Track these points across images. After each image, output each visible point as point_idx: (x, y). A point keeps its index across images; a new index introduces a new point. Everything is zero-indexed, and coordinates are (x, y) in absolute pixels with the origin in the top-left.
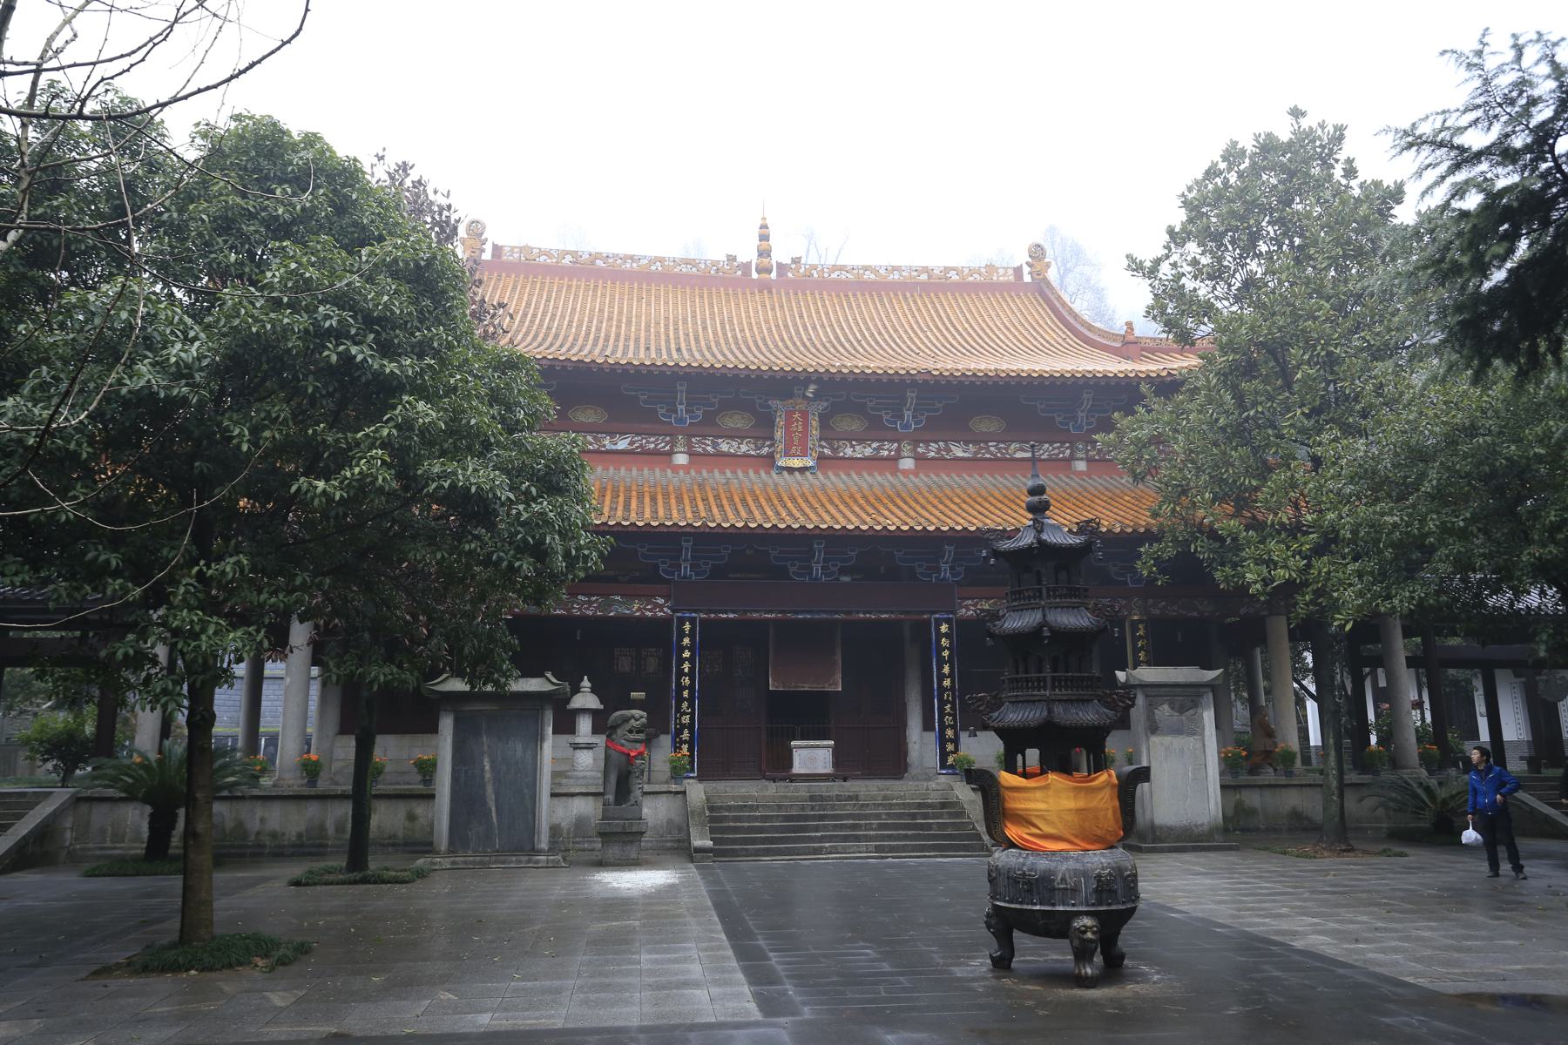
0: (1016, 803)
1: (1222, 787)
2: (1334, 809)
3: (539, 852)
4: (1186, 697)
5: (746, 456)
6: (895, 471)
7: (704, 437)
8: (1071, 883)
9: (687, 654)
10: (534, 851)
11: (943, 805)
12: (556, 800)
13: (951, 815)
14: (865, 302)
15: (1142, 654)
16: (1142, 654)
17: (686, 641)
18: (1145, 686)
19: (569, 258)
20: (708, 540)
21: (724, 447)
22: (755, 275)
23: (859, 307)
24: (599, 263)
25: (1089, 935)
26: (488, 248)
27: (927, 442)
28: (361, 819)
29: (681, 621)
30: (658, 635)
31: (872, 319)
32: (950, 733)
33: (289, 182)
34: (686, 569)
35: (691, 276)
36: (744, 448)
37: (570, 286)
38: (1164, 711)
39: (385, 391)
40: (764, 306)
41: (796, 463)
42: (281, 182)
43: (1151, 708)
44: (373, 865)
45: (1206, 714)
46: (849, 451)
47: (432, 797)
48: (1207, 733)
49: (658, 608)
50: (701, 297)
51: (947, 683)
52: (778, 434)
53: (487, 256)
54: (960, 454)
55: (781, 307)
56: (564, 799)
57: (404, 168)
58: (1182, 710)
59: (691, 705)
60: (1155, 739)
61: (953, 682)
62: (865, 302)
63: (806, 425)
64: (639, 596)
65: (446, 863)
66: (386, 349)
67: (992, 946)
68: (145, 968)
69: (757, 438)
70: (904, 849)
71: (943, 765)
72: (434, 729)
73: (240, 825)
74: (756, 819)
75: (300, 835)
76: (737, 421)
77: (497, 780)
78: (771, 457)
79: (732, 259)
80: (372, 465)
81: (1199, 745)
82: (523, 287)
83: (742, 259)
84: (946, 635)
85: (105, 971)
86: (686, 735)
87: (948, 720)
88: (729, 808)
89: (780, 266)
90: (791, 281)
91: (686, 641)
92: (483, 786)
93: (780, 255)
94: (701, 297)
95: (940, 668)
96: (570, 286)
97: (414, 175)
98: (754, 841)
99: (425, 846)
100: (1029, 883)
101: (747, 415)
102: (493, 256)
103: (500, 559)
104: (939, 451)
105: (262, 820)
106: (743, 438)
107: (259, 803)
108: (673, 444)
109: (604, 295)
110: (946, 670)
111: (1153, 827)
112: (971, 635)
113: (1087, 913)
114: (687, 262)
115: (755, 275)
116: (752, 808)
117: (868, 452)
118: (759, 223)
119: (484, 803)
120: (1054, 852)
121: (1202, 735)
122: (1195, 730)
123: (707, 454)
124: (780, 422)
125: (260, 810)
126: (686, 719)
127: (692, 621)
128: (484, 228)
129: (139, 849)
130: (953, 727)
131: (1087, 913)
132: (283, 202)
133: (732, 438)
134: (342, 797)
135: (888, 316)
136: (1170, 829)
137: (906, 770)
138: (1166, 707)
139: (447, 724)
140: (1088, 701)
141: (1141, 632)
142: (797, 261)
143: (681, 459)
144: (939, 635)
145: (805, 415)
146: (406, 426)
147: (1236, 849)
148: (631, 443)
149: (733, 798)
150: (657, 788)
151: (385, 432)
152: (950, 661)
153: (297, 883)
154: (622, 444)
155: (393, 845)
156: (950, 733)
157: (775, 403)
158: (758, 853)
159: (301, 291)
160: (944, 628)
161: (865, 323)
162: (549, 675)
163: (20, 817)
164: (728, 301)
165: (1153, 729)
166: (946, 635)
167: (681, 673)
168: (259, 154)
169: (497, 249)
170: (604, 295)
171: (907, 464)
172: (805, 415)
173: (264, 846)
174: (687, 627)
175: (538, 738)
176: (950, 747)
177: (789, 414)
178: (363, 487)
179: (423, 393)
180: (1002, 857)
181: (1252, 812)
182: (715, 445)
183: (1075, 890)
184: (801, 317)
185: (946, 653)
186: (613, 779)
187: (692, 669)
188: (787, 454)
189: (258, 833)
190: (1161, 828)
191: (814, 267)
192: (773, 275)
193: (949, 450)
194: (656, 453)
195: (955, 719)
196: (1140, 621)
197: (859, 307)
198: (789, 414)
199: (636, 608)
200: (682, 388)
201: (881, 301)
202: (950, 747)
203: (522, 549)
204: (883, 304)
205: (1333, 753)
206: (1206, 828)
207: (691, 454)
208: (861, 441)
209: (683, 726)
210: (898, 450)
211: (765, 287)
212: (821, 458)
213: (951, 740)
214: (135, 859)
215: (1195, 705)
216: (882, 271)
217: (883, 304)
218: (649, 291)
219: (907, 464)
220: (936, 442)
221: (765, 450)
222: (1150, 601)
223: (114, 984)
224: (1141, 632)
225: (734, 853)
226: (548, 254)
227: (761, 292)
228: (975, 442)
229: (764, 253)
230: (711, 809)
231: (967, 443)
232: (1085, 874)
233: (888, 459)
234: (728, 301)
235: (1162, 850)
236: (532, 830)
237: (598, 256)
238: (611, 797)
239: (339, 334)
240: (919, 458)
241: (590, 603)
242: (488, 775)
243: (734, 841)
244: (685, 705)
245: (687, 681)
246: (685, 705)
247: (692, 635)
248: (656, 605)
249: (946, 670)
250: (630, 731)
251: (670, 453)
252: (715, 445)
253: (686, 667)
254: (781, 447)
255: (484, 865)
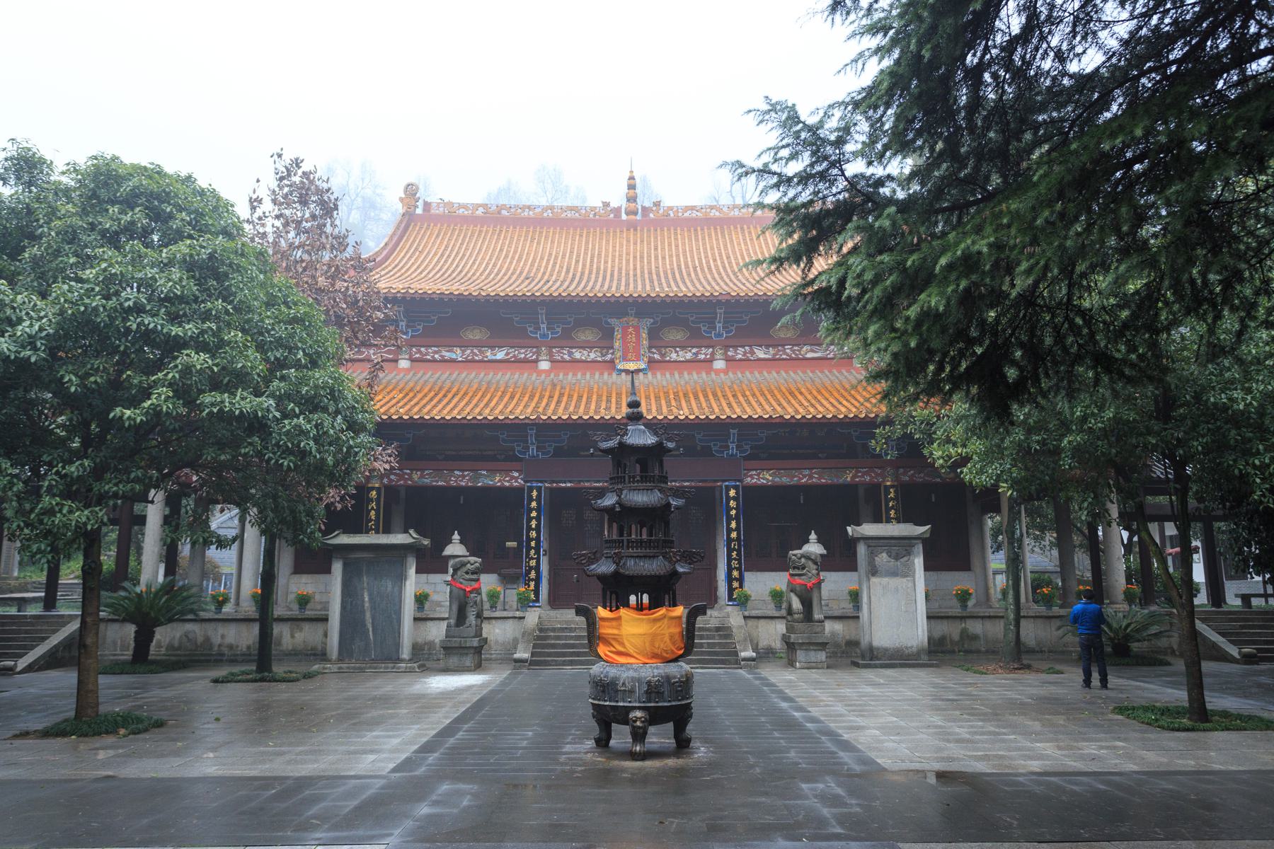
0: (606, 630)
1: (928, 618)
2: (1011, 636)
3: (402, 661)
4: (900, 547)
5: (593, 361)
6: (710, 370)
7: (562, 348)
8: (629, 686)
9: (534, 514)
10: (399, 660)
11: (718, 629)
12: (420, 624)
13: (721, 637)
14: (710, 235)
15: (892, 512)
16: (892, 512)
17: (534, 504)
18: (866, 539)
19: (481, 210)
20: (547, 430)
21: (577, 355)
22: (624, 217)
23: (703, 239)
24: (504, 212)
25: (638, 723)
26: (420, 204)
27: (735, 347)
28: (265, 637)
29: (531, 489)
30: (513, 500)
31: (712, 248)
32: (735, 573)
33: (120, 203)
34: (533, 450)
35: (575, 220)
36: (592, 356)
37: (480, 231)
38: (883, 559)
39: (174, 346)
40: (628, 241)
41: (632, 366)
42: (113, 203)
43: (872, 556)
44: (278, 669)
45: (916, 561)
46: (674, 356)
47: (327, 620)
48: (917, 576)
49: (514, 480)
50: (581, 236)
51: (734, 535)
52: (617, 344)
53: (419, 211)
54: (762, 355)
55: (642, 241)
56: (437, 622)
57: (297, 163)
58: (897, 558)
59: (538, 552)
60: (874, 580)
61: (739, 534)
62: (710, 235)
63: (638, 337)
64: (500, 471)
65: (334, 668)
66: (174, 318)
67: (596, 731)
68: (46, 734)
69: (602, 348)
70: (708, 662)
71: (730, 598)
72: (328, 571)
73: (207, 639)
74: (571, 638)
75: (249, 647)
76: (588, 335)
77: (373, 608)
78: (612, 361)
79: (606, 204)
80: (161, 398)
81: (910, 584)
82: (445, 234)
83: (614, 204)
84: (734, 498)
85: (25, 734)
86: (533, 574)
87: (734, 564)
88: (554, 630)
89: (644, 208)
90: (652, 220)
91: (534, 504)
92: (363, 612)
93: (644, 201)
94: (581, 236)
95: (729, 524)
96: (480, 231)
97: (305, 167)
98: (564, 655)
99: (321, 655)
100: (603, 686)
101: (595, 330)
102: (424, 210)
103: (270, 459)
104: (745, 353)
105: (223, 636)
106: (591, 348)
107: (220, 624)
108: (538, 354)
109: (505, 238)
110: (733, 525)
111: (871, 648)
112: (752, 496)
113: (639, 708)
114: (572, 209)
115: (624, 217)
116: (571, 630)
117: (689, 356)
118: (628, 175)
119: (364, 625)
120: (622, 665)
121: (914, 576)
122: (908, 573)
123: (564, 361)
124: (618, 335)
125: (222, 629)
126: (533, 563)
127: (539, 489)
128: (417, 188)
129: (128, 655)
130: (739, 569)
131: (639, 708)
132: (113, 216)
133: (583, 348)
134: (281, 620)
135: (725, 246)
136: (886, 650)
137: (716, 602)
138: (884, 555)
139: (337, 567)
140: (654, 557)
141: (892, 495)
142: (657, 204)
143: (544, 365)
144: (728, 499)
145: (637, 329)
146: (187, 370)
147: (937, 666)
148: (507, 354)
149: (560, 622)
150: (505, 614)
151: (170, 376)
152: (737, 518)
153: (216, 681)
154: (500, 355)
155: (315, 655)
156: (735, 573)
157: (613, 321)
158: (564, 663)
159: (111, 286)
160: (732, 493)
161: (706, 252)
162: (411, 531)
163: (55, 632)
164: (601, 239)
165: (874, 571)
166: (734, 498)
167: (529, 528)
168: (104, 182)
169: (427, 205)
170: (505, 238)
171: (719, 364)
172: (637, 329)
173: (223, 655)
174: (535, 493)
175: (402, 578)
176: (735, 584)
177: (625, 330)
178: (156, 412)
179: (201, 347)
180: (596, 669)
181: (975, 638)
182: (570, 354)
183: (632, 692)
184: (656, 249)
185: (733, 512)
186: (455, 608)
187: (538, 526)
188: (625, 359)
189: (220, 645)
190: (878, 649)
191: (671, 208)
192: (639, 217)
193: (753, 353)
194: (525, 361)
195: (740, 563)
196: (892, 486)
197: (703, 239)
198: (625, 330)
199: (497, 480)
200: (542, 312)
201: (723, 233)
202: (735, 584)
203: (287, 452)
204: (723, 236)
205: (1011, 592)
206: (915, 650)
207: (552, 361)
208: (683, 348)
209: (531, 568)
210: (713, 354)
211: (632, 226)
212: (651, 361)
213: (736, 579)
214: (124, 663)
215: (909, 553)
216: (725, 209)
217: (723, 236)
218: (541, 233)
219: (719, 364)
220: (743, 346)
221: (609, 357)
222: (901, 470)
223: (30, 742)
224: (892, 495)
225: (546, 663)
226: (465, 207)
227: (628, 230)
228: (774, 346)
229: (632, 199)
230: (541, 630)
231: (768, 346)
232: (639, 680)
233: (704, 361)
234: (601, 239)
235: (876, 666)
236: (398, 645)
237: (503, 207)
238: (452, 621)
239: (138, 309)
240: (728, 360)
241: (464, 477)
242: (367, 605)
243: (550, 655)
244: (533, 552)
245: (534, 534)
246: (533, 552)
247: (538, 499)
248: (513, 478)
249: (733, 525)
250: (467, 573)
251: (536, 361)
252: (570, 354)
253: (534, 523)
254: (619, 354)
255: (362, 670)
